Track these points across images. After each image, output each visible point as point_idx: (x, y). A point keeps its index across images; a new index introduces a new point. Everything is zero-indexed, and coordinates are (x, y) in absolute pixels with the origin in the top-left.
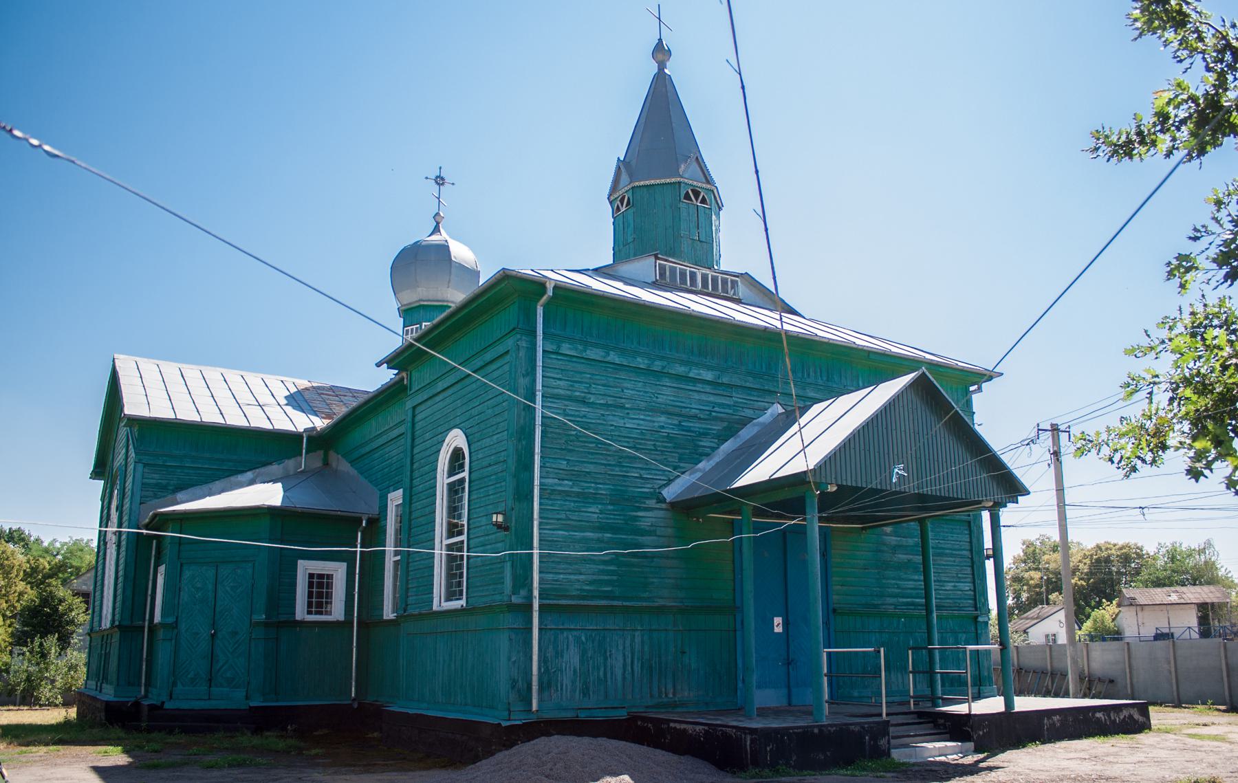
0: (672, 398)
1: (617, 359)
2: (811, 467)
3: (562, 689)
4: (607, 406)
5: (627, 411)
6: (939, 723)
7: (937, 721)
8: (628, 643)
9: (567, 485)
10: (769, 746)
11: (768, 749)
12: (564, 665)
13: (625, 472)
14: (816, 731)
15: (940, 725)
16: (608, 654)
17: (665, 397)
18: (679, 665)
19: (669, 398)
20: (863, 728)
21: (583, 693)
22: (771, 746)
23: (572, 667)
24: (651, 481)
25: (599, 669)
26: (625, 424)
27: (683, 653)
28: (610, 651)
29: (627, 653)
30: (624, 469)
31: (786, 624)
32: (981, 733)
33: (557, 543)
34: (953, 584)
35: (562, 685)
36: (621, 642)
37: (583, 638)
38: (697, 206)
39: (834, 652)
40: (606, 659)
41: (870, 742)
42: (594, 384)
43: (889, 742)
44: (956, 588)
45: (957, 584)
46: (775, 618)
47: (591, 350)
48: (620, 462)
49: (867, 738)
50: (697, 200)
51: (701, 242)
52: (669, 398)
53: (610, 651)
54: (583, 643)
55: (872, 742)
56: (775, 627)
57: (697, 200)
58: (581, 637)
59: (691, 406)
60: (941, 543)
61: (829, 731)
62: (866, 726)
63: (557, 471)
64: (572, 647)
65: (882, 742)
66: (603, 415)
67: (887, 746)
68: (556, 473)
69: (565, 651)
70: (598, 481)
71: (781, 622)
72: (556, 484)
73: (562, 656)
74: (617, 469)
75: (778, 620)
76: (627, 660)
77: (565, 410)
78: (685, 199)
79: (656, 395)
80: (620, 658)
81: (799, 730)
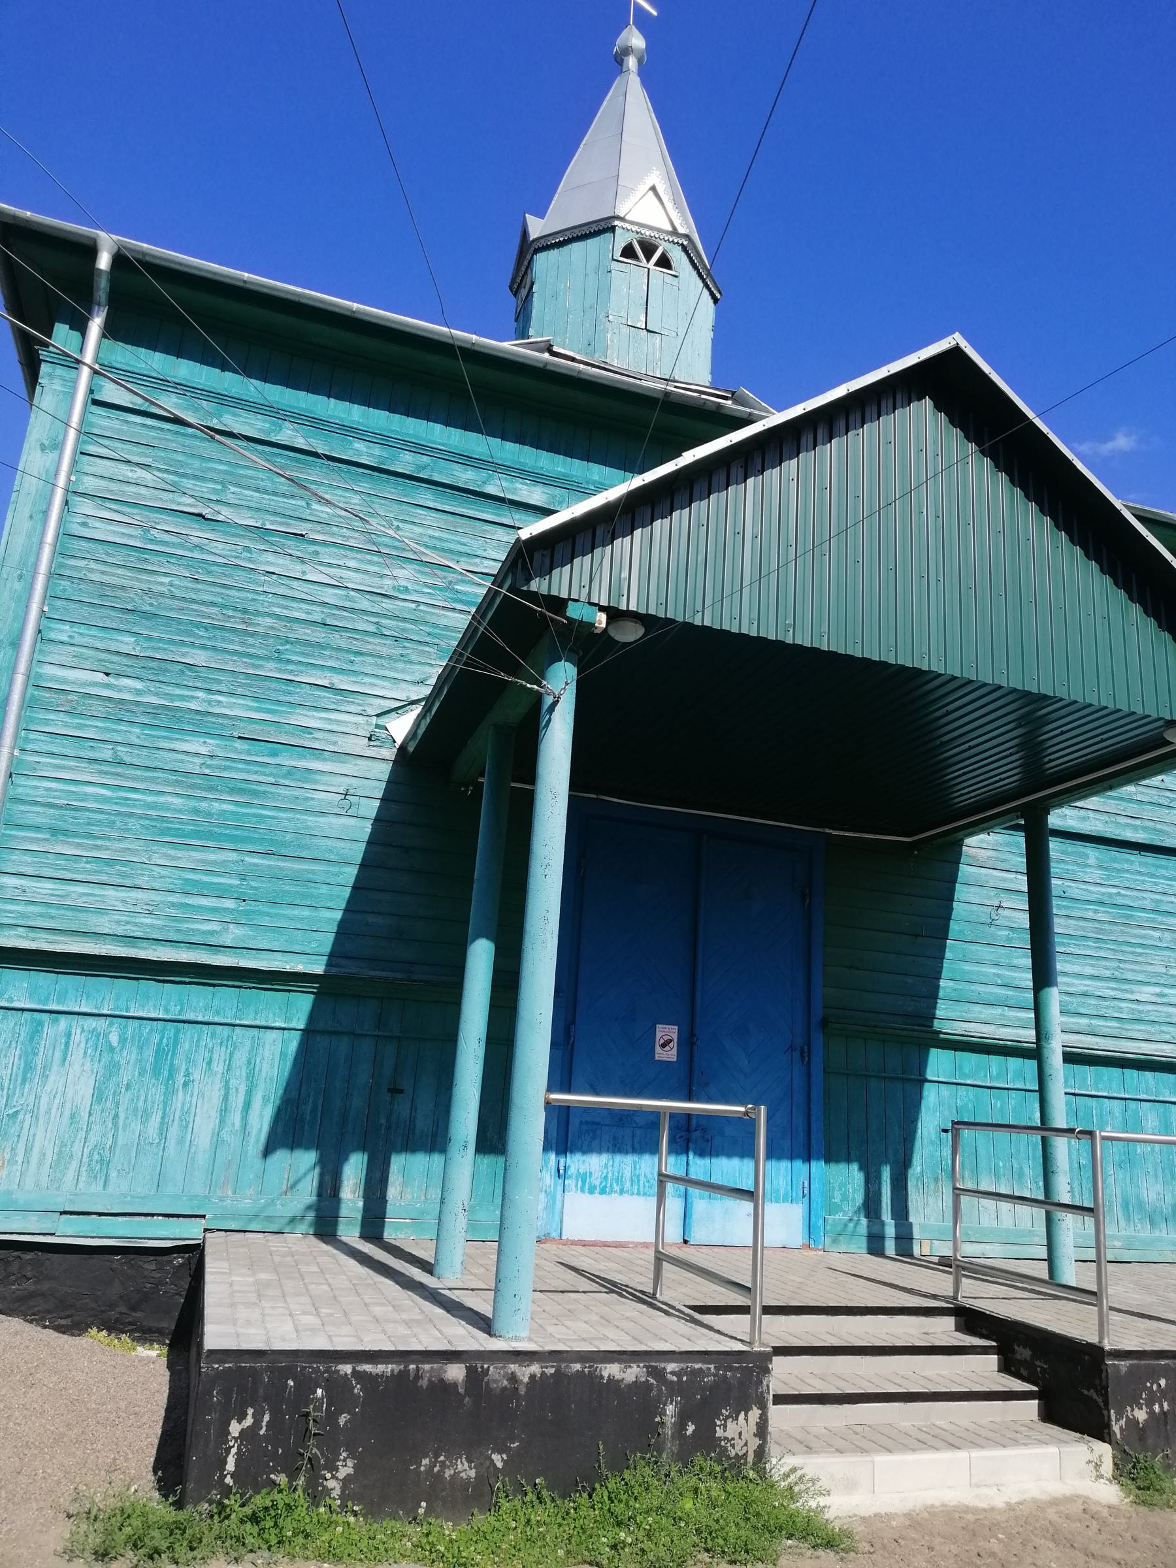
0: (437, 534)
1: (302, 441)
2: (559, 568)
3: (27, 1160)
4: (260, 532)
5: (313, 548)
6: (1018, 1356)
7: (1014, 1352)
8: (241, 1057)
9: (127, 687)
10: (242, 1417)
11: (235, 1428)
12: (45, 1100)
13: (291, 672)
14: (456, 1372)
15: (1020, 1361)
16: (180, 1079)
17: (419, 530)
18: (383, 1121)
19: (431, 532)
20: (659, 1374)
21: (91, 1170)
22: (249, 1421)
23: (68, 1105)
24: (358, 699)
25: (146, 1116)
26: (304, 573)
27: (395, 1091)
28: (188, 1074)
29: (233, 1083)
30: (290, 667)
31: (688, 1043)
32: (1141, 1415)
33: (78, 814)
34: (1157, 990)
35: (28, 1150)
36: (220, 1054)
37: (114, 1039)
38: (649, 269)
39: (587, 1109)
40: (170, 1093)
41: (681, 1426)
42: (235, 485)
43: (762, 1430)
44: (1165, 1000)
45: (1166, 991)
46: (659, 1027)
47: (235, 415)
48: (278, 651)
49: (670, 1409)
50: (648, 261)
51: (649, 331)
52: (431, 532)
53: (188, 1074)
54: (112, 1049)
55: (691, 1428)
56: (658, 1047)
57: (648, 261)
58: (106, 1036)
59: (484, 554)
60: (1123, 896)
61: (513, 1378)
62: (671, 1367)
63: (103, 656)
64: (77, 1055)
65: (732, 1429)
66: (248, 549)
67: (755, 1443)
68: (101, 660)
69: (55, 1068)
70: (216, 687)
71: (675, 1037)
72: (96, 684)
73: (45, 1077)
74: (271, 665)
75: (667, 1032)
76: (232, 1098)
77: (147, 529)
78: (622, 255)
79: (396, 523)
80: (215, 1094)
81: (380, 1368)
